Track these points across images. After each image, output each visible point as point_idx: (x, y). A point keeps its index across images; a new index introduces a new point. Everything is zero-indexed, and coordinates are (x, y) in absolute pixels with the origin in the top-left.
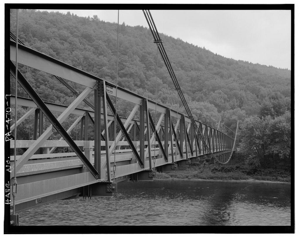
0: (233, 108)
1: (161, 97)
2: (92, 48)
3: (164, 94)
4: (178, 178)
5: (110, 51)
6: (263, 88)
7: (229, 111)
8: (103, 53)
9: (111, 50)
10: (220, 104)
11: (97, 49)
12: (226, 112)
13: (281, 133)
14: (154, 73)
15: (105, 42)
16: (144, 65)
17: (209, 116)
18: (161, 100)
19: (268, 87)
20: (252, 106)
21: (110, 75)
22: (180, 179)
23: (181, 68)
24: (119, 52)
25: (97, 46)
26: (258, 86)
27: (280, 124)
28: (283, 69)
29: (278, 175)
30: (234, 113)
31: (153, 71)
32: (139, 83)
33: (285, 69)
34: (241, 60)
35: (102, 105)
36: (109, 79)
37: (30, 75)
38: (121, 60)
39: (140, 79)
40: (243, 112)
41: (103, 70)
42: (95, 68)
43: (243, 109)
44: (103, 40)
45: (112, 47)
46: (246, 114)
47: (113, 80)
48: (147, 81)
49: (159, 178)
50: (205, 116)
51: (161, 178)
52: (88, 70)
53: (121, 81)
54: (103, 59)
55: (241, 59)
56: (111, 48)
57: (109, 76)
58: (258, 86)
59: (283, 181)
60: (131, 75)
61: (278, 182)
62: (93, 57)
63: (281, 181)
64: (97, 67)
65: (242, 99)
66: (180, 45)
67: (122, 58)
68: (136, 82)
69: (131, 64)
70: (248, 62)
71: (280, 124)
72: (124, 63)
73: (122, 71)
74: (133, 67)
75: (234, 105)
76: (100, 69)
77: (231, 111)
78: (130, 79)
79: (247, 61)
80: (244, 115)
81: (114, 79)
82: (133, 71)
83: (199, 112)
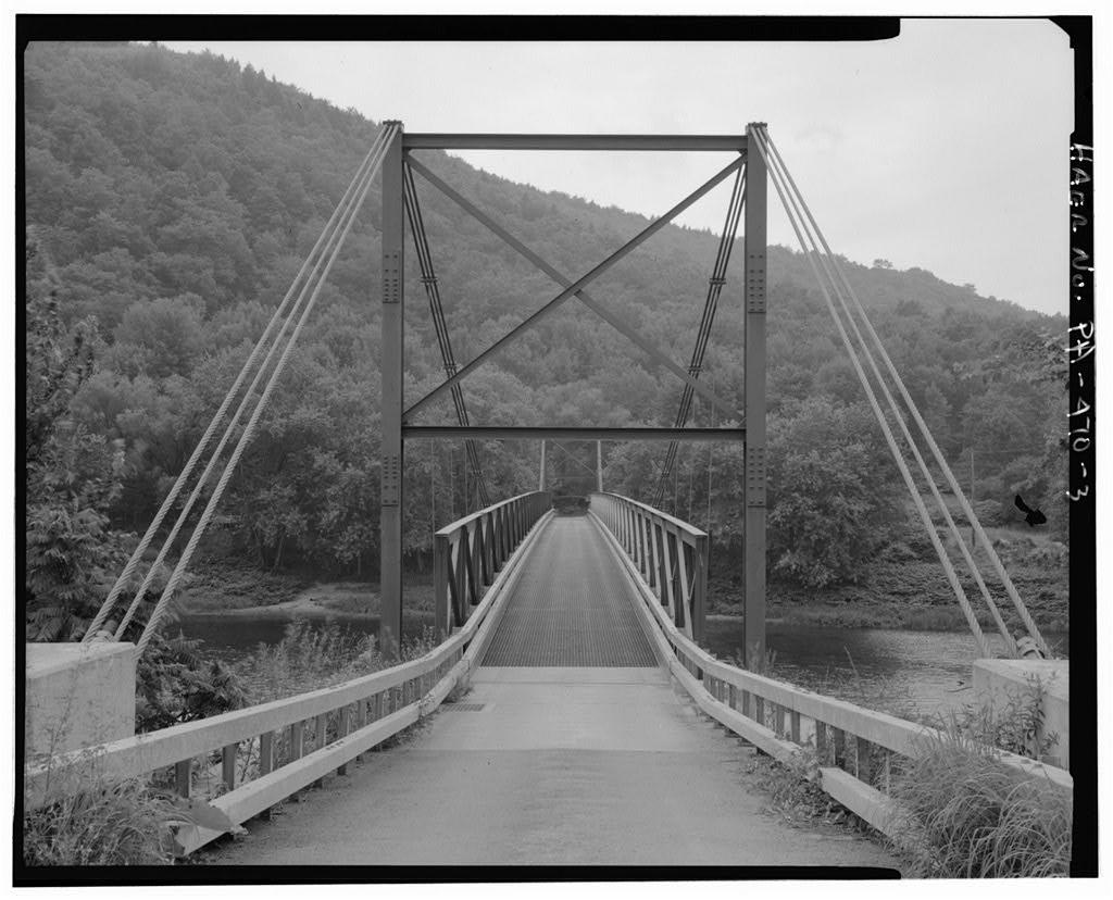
0: (560, 378)
1: (329, 335)
2: (48, 133)
3: (337, 324)
4: (421, 609)
5: (117, 150)
6: (647, 310)
7: (549, 390)
8: (89, 154)
9: (119, 143)
10: (519, 363)
11: (65, 137)
12: (539, 392)
13: (724, 474)
14: (283, 238)
15: (94, 112)
16: (241, 209)
17: (511, 417)
18: (331, 347)
19: (663, 309)
20: (620, 374)
21: (127, 241)
22: (426, 613)
23: (372, 222)
24: (150, 153)
25: (66, 125)
26: (632, 304)
27: (722, 448)
28: (697, 232)
29: (716, 597)
30: (565, 398)
31: (279, 231)
32: (231, 275)
33: (703, 232)
34: (559, 190)
35: (613, 551)
36: (126, 257)
37: (136, 352)
38: (163, 186)
39: (333, 316)
40: (594, 394)
41: (100, 220)
42: (67, 214)
43: (596, 384)
44: (88, 107)
45: (120, 133)
46: (606, 400)
47: (137, 261)
48: (259, 267)
49: (360, 612)
50: (500, 415)
51: (366, 611)
52: (41, 218)
53: (168, 266)
54: (95, 179)
55: (559, 190)
56: (119, 137)
57: (122, 245)
58: (632, 304)
59: (730, 613)
60: (204, 245)
61: (719, 617)
62: (58, 172)
63: (724, 614)
64: (76, 208)
65: (588, 345)
66: (360, 135)
67: (168, 181)
68: (222, 272)
69: (203, 205)
70: (582, 200)
71: (722, 448)
72: (178, 201)
73: (168, 229)
74: (209, 215)
75: (563, 368)
76: (86, 215)
77: (559, 388)
78: (201, 261)
79: (579, 197)
80: (599, 403)
81: (143, 258)
82: (211, 230)
83: (480, 402)
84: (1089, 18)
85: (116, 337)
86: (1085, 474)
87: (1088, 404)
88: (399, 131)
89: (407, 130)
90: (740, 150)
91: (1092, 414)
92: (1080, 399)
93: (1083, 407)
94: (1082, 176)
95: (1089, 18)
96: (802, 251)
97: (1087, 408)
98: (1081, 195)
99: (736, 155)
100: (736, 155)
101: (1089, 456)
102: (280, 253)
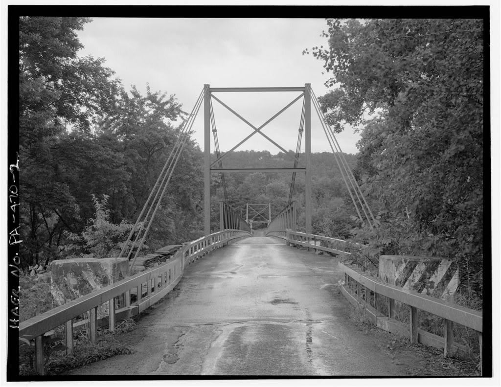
47: (73, 61)
84: (9, 6)
85: (348, 240)
86: (14, 181)
87: (12, 274)
88: (209, 87)
89: (211, 87)
90: (303, 91)
91: (9, 204)
92: (15, 211)
93: (13, 207)
94: (15, 311)
95: (9, 6)
96: (203, 150)
97: (12, 207)
98: (14, 260)
99: (303, 92)
100: (303, 92)
101: (10, 316)
102: (91, 71)
